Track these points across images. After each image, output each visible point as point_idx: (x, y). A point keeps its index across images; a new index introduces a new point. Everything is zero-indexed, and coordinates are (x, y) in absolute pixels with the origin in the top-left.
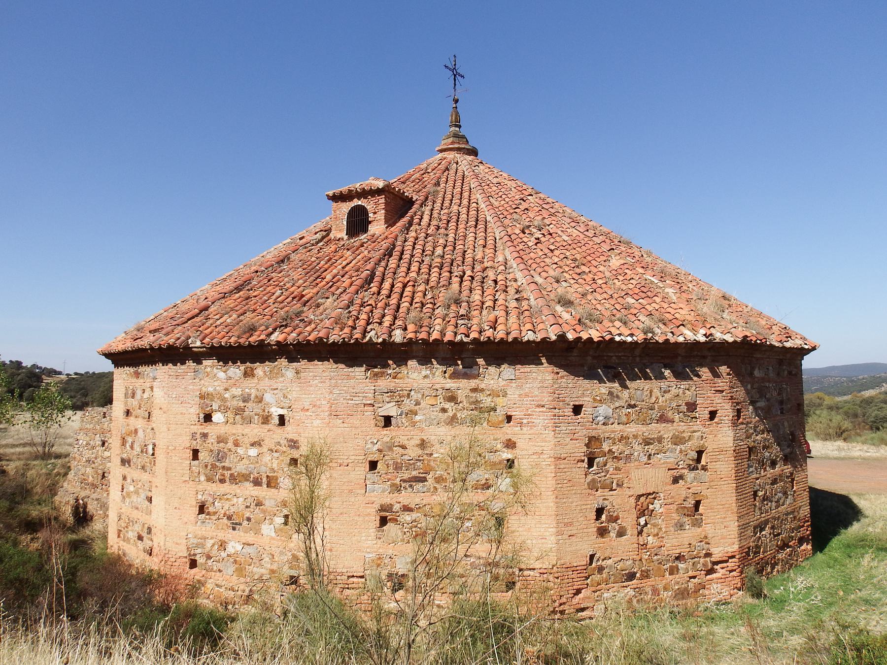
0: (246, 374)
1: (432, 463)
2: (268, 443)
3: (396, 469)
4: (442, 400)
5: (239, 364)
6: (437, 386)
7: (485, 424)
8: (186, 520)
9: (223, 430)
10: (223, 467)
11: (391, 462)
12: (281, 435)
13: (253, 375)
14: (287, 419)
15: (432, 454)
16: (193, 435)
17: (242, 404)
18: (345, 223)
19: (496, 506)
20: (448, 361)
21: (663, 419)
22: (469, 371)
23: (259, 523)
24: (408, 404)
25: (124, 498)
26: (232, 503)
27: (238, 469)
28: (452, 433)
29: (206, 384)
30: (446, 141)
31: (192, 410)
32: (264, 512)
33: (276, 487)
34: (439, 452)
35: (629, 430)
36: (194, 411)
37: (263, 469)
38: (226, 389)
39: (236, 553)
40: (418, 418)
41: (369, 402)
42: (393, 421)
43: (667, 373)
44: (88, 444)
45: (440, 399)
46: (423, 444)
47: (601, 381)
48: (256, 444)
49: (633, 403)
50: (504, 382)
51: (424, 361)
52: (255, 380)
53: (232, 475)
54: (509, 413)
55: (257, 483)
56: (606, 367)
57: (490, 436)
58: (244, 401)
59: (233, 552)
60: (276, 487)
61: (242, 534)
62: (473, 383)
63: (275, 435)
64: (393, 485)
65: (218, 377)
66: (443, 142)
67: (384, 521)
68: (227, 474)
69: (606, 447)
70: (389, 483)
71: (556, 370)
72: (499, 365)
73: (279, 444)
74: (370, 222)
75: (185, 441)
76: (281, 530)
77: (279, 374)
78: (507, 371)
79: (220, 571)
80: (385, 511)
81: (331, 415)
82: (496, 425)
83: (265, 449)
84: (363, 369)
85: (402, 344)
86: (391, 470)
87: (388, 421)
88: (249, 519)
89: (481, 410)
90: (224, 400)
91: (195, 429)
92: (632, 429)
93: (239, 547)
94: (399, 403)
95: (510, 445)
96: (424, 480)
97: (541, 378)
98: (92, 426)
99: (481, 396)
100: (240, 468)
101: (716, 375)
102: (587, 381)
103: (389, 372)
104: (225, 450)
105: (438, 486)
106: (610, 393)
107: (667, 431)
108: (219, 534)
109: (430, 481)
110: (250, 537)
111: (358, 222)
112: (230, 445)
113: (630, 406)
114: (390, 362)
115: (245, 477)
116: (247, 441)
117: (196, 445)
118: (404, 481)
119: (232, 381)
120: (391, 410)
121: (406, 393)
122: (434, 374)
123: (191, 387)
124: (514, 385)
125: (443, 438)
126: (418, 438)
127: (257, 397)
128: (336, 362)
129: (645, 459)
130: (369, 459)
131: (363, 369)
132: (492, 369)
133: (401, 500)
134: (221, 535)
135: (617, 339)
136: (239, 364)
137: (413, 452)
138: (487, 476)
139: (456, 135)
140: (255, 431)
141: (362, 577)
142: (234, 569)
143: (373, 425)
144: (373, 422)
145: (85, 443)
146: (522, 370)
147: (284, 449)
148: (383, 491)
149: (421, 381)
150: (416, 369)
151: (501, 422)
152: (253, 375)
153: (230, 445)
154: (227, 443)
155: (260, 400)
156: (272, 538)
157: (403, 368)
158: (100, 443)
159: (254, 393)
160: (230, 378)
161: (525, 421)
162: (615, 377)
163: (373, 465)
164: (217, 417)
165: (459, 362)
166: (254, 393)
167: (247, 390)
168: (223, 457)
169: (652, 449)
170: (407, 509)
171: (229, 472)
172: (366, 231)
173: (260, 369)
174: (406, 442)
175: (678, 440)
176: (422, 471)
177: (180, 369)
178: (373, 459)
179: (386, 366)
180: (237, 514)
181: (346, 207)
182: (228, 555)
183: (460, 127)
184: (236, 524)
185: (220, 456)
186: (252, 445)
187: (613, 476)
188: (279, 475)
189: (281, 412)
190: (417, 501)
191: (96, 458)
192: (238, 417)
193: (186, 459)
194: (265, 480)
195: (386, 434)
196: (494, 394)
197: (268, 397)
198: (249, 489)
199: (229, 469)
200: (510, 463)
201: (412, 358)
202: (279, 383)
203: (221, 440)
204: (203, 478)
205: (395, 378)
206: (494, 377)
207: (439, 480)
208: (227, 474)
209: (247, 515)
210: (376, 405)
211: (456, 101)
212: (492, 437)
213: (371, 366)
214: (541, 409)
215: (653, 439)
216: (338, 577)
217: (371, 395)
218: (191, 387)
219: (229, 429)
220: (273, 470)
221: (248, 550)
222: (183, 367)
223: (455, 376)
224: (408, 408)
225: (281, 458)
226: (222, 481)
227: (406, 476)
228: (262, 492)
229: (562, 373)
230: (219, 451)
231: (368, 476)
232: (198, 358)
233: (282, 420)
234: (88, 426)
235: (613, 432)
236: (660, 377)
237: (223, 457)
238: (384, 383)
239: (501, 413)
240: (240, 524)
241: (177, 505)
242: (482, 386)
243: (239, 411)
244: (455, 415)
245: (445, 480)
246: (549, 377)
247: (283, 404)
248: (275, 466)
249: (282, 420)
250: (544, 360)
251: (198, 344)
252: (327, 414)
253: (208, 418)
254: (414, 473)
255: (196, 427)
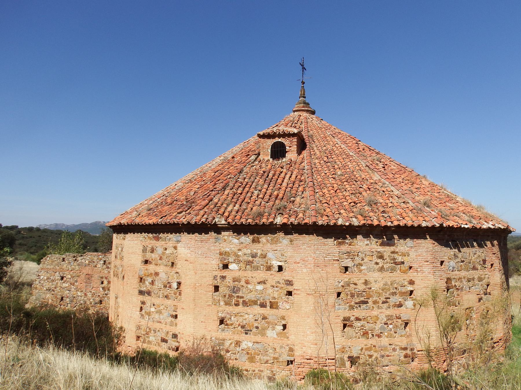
0: (254, 241)
1: (371, 293)
2: (271, 281)
3: (351, 296)
4: (376, 258)
5: (249, 235)
6: (373, 250)
7: (399, 271)
8: (210, 329)
9: (237, 274)
10: (238, 297)
11: (349, 293)
12: (280, 277)
13: (259, 242)
14: (284, 268)
15: (371, 288)
16: (215, 278)
17: (250, 259)
18: (270, 151)
19: (405, 317)
20: (378, 236)
21: (474, 268)
22: (390, 242)
23: (264, 329)
24: (358, 260)
25: (142, 315)
26: (245, 318)
27: (248, 297)
28: (382, 276)
29: (225, 246)
30: (298, 105)
31: (214, 262)
32: (268, 323)
33: (277, 308)
34: (375, 287)
35: (462, 274)
36: (215, 262)
37: (267, 297)
38: (239, 250)
39: (249, 348)
40: (363, 268)
41: (336, 259)
42: (349, 269)
43: (475, 244)
44: (48, 278)
45: (375, 257)
46: (366, 283)
47: (451, 249)
48: (263, 282)
49: (463, 260)
50: (409, 248)
51: (366, 236)
52: (261, 245)
53: (244, 301)
54: (411, 265)
55: (263, 305)
56: (453, 241)
57: (399, 277)
58: (252, 257)
59: (246, 347)
60: (277, 308)
61: (253, 337)
62: (392, 248)
63: (274, 277)
64: (350, 306)
65: (230, 242)
66: (296, 106)
67: (345, 326)
68: (241, 300)
69: (453, 283)
70: (348, 305)
71: (434, 242)
72: (405, 239)
73: (278, 282)
74: (287, 152)
75: (209, 282)
76: (281, 333)
77: (277, 242)
78: (409, 242)
79: (236, 359)
80: (346, 320)
81: (315, 266)
82: (404, 272)
83: (268, 285)
84: (333, 240)
85: (357, 227)
86: (349, 297)
87: (346, 269)
88: (257, 328)
89: (396, 263)
90: (238, 256)
91: (216, 273)
92: (463, 273)
93: (250, 345)
94: (353, 260)
95: (412, 283)
96: (366, 302)
97: (427, 245)
98: (52, 267)
99: (396, 256)
100: (251, 297)
101: (493, 245)
102: (445, 248)
103: (347, 241)
104: (239, 286)
105: (374, 306)
106: (455, 255)
107: (475, 274)
108: (235, 337)
109: (370, 303)
110: (259, 338)
111: (278, 151)
112: (243, 283)
113: (463, 262)
114: (348, 236)
115: (255, 303)
116: (255, 281)
117: (218, 282)
118: (356, 303)
119: (244, 245)
120: (348, 263)
121: (356, 254)
122: (371, 243)
123: (213, 248)
124: (413, 250)
125: (378, 280)
126: (364, 279)
127: (262, 255)
128: (317, 236)
129: (468, 289)
130: (337, 291)
131: (333, 240)
132: (402, 241)
133: (354, 314)
134: (237, 338)
135: (463, 226)
136: (249, 235)
137: (361, 287)
138: (400, 300)
139: (305, 103)
140: (261, 275)
141: (333, 359)
142: (247, 358)
143: (339, 272)
144: (339, 270)
145: (46, 278)
146: (417, 242)
147: (283, 286)
148: (345, 309)
149: (365, 247)
150: (361, 240)
151: (407, 270)
152: (259, 242)
153: (243, 283)
154: (240, 282)
155: (264, 256)
156: (275, 339)
157: (355, 239)
158: (59, 278)
159: (259, 252)
160: (242, 243)
161: (419, 270)
162: (456, 246)
163: (339, 294)
164: (231, 266)
165: (385, 237)
166: (259, 252)
167: (255, 251)
168: (237, 290)
169: (471, 284)
170: (358, 319)
171: (242, 299)
172: (284, 156)
173: (263, 238)
174: (357, 282)
175: (480, 279)
176: (365, 297)
177: (204, 236)
178: (339, 291)
179: (345, 238)
180: (249, 324)
181: (270, 142)
182: (242, 350)
183: (305, 97)
184: (248, 330)
185: (235, 290)
186: (259, 283)
187: (457, 299)
188: (279, 301)
189: (280, 264)
190: (364, 314)
191: (55, 288)
192: (248, 266)
193: (209, 292)
194: (268, 304)
195: (346, 277)
196: (404, 255)
197: (270, 255)
198: (257, 310)
199: (242, 297)
200: (411, 292)
201: (359, 234)
202: (278, 247)
203: (235, 280)
204: (222, 303)
205: (350, 245)
206: (403, 246)
207: (375, 302)
208: (241, 300)
209: (256, 325)
210: (340, 260)
211: (303, 83)
212: (402, 278)
213: (337, 238)
214: (427, 263)
215: (470, 279)
216: (321, 360)
217: (337, 255)
218: (213, 248)
219: (241, 274)
220: (274, 298)
221: (258, 346)
222: (206, 236)
223: (382, 244)
224: (358, 262)
225: (280, 291)
226: (237, 305)
227: (357, 301)
228: (267, 311)
229: (436, 244)
230: (234, 287)
231: (337, 301)
232: (217, 229)
233: (280, 268)
234: (49, 267)
235: (456, 275)
236: (473, 246)
237: (237, 290)
238: (345, 248)
239: (407, 265)
240: (251, 331)
241: (203, 320)
242: (397, 250)
243: (249, 263)
244: (383, 266)
245: (378, 303)
246: (431, 246)
247: (281, 259)
248: (276, 295)
249: (280, 268)
250: (428, 237)
251: (223, 222)
252: (312, 265)
253: (226, 267)
254: (362, 299)
255: (217, 272)
